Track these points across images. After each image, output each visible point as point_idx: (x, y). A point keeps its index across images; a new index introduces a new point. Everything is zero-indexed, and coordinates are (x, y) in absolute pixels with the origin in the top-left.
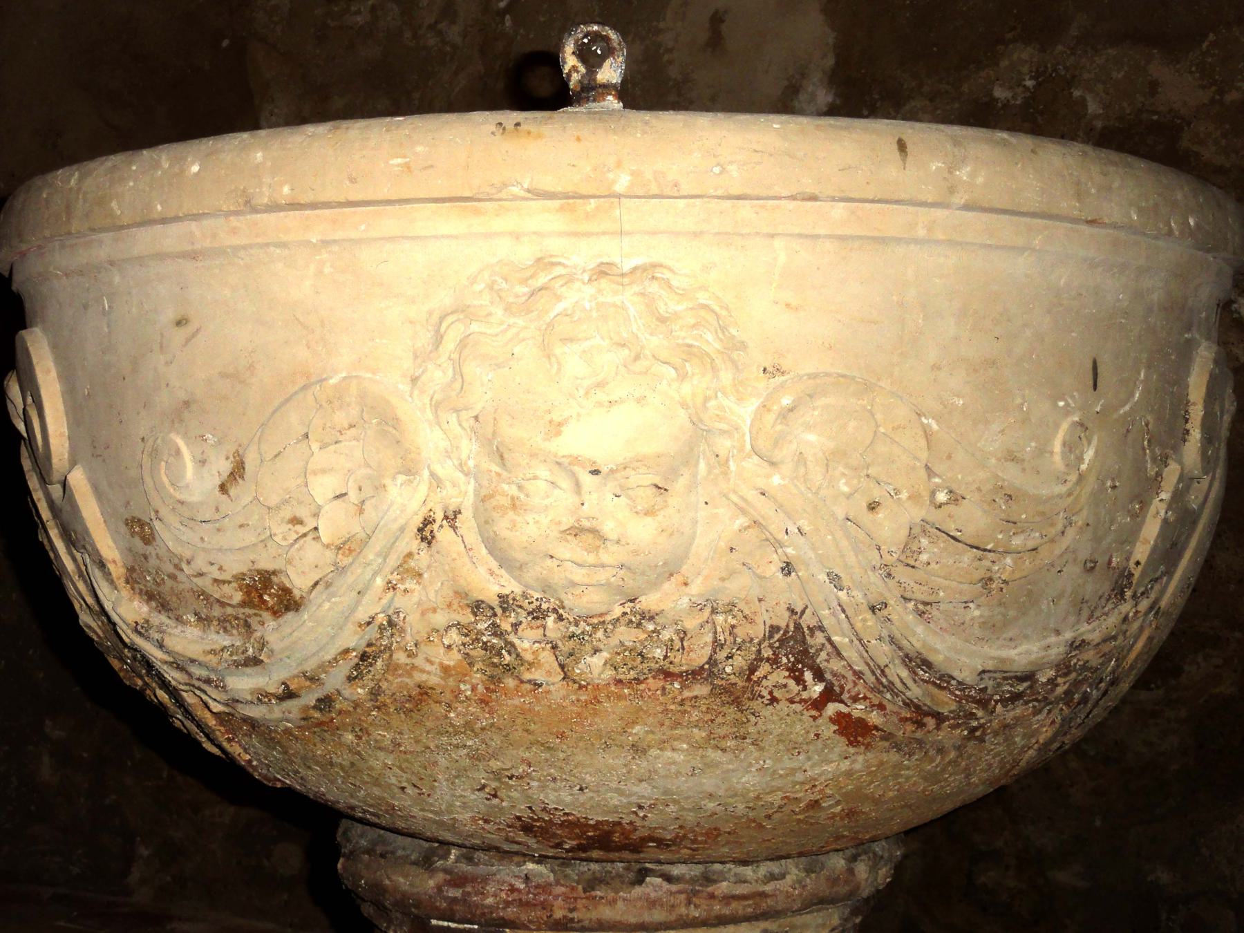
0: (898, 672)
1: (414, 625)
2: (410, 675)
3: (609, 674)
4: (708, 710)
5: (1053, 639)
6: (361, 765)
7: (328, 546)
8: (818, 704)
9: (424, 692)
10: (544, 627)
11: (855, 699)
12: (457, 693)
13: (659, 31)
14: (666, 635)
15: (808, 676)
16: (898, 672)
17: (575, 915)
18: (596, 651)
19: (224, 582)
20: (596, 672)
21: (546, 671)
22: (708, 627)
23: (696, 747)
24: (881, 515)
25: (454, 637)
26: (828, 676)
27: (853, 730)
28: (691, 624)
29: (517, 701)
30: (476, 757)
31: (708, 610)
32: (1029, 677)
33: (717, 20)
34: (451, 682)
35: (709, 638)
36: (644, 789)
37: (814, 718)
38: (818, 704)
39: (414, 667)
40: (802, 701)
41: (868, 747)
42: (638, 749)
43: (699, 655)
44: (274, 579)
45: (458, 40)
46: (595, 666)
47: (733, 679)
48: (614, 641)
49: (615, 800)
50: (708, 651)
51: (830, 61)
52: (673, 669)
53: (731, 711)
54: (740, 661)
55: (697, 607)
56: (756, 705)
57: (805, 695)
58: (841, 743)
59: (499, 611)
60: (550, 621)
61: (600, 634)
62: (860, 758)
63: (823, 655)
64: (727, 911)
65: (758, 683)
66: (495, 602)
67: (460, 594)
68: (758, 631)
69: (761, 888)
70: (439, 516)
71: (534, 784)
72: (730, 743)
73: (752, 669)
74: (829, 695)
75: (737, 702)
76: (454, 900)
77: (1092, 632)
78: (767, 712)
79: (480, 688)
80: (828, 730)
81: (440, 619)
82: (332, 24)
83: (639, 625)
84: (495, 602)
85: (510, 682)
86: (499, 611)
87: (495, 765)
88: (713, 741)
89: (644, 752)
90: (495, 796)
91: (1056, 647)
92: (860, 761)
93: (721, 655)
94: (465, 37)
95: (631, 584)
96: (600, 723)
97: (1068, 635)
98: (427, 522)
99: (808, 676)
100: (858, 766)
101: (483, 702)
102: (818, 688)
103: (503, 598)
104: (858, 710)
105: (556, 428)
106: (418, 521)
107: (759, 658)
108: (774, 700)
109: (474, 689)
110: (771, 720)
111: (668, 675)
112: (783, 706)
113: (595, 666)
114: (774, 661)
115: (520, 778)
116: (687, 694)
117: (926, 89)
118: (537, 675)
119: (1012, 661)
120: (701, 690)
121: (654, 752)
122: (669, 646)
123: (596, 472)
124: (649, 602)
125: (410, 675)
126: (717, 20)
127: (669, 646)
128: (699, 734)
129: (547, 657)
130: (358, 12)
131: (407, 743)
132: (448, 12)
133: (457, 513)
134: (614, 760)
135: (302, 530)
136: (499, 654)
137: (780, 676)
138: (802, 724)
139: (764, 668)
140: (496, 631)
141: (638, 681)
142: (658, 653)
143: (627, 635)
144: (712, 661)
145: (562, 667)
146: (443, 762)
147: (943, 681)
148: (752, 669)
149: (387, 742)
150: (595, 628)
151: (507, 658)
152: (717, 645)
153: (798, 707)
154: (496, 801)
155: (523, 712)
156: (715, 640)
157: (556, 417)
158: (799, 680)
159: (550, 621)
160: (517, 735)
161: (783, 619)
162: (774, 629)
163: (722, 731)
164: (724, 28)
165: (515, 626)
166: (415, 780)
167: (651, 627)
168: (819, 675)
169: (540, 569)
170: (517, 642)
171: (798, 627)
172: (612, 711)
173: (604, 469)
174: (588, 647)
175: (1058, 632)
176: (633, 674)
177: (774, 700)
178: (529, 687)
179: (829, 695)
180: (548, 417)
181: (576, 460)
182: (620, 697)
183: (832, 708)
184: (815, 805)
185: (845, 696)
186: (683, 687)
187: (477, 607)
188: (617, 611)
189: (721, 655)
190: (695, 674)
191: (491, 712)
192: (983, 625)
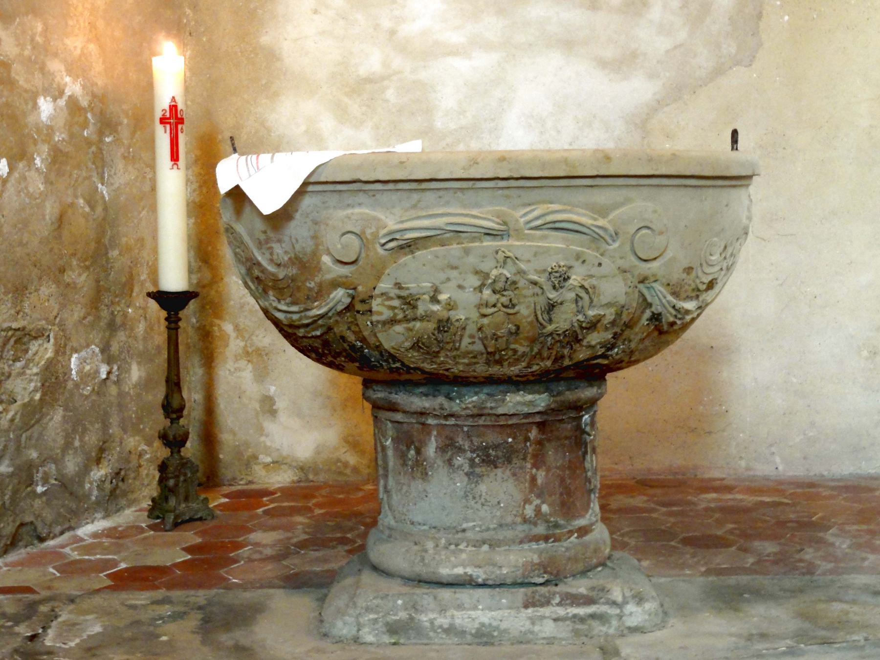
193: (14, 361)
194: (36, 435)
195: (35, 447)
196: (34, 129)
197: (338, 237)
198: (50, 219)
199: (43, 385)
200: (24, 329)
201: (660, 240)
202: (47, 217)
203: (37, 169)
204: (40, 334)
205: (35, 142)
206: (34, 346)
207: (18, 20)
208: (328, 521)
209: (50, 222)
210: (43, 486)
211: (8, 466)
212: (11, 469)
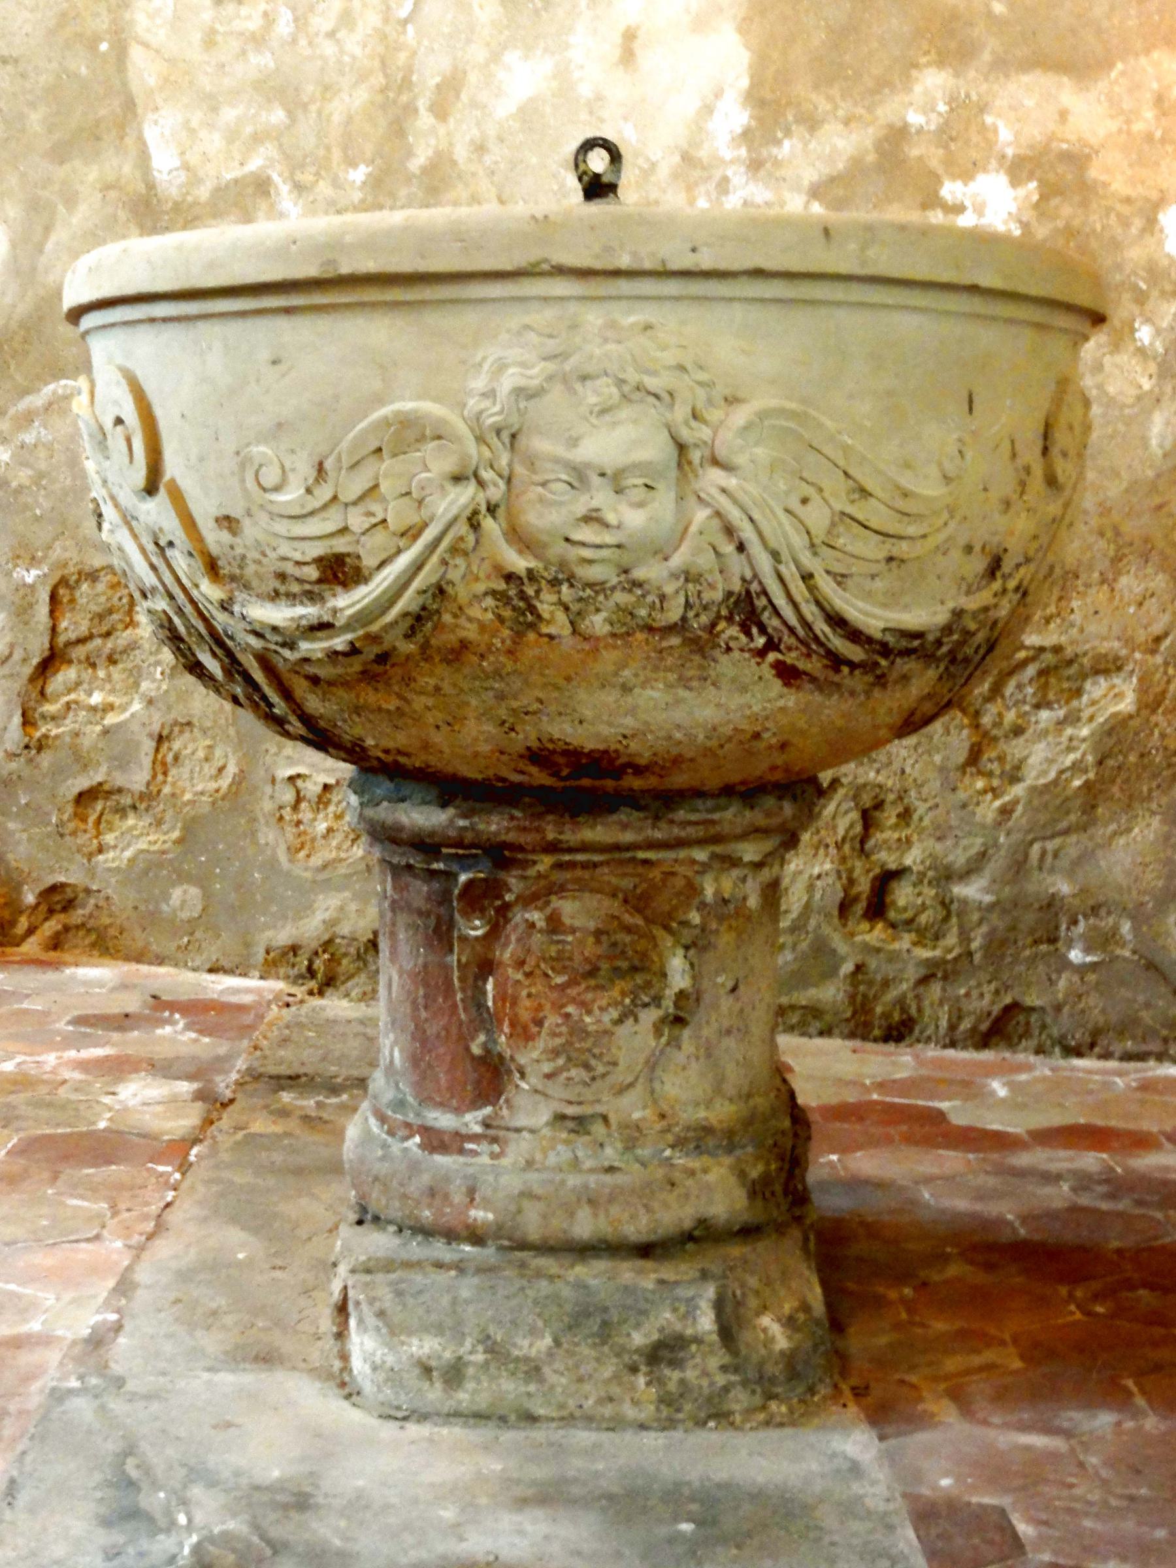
0: (821, 627)
1: (462, 593)
2: (453, 631)
3: (607, 628)
4: (680, 657)
5: (939, 608)
6: (407, 709)
7: (394, 534)
8: (761, 653)
9: (464, 645)
10: (559, 592)
11: (790, 649)
12: (490, 646)
13: (567, 46)
14: (650, 599)
15: (755, 630)
16: (821, 627)
17: (562, 837)
18: (598, 610)
19: (305, 564)
20: (597, 627)
21: (559, 624)
22: (682, 593)
23: (669, 686)
24: (809, 507)
25: (489, 602)
26: (770, 630)
27: (788, 674)
28: (669, 589)
29: (537, 651)
30: (501, 697)
31: (682, 579)
32: (919, 635)
33: (630, 36)
34: (486, 637)
35: (682, 600)
36: (629, 721)
37: (758, 664)
38: (761, 653)
39: (457, 626)
40: (750, 650)
41: (798, 688)
42: (626, 689)
43: (674, 614)
44: (348, 560)
45: (358, 51)
46: (598, 623)
47: (700, 633)
48: (611, 603)
49: (605, 730)
50: (681, 611)
51: (745, 83)
52: (655, 625)
53: (697, 658)
54: (704, 619)
55: (674, 576)
56: (717, 653)
57: (752, 645)
58: (778, 683)
59: (526, 580)
60: (565, 588)
61: (601, 598)
62: (793, 698)
63: (766, 614)
64: (683, 834)
65: (718, 635)
66: (523, 574)
67: (497, 568)
68: (718, 595)
69: (709, 816)
70: (483, 508)
71: (545, 718)
72: (695, 684)
73: (713, 625)
74: (771, 645)
75: (701, 651)
76: (465, 828)
77: (972, 603)
78: (724, 659)
79: (508, 642)
80: (767, 672)
81: (480, 587)
82: (221, 29)
83: (630, 591)
84: (523, 574)
85: (531, 636)
86: (526, 580)
87: (515, 704)
88: (684, 681)
89: (631, 690)
90: (512, 729)
91: (941, 617)
92: (791, 699)
93: (691, 614)
94: (365, 46)
95: (626, 558)
96: (598, 668)
97: (951, 605)
98: (475, 513)
99: (755, 630)
100: (791, 704)
101: (510, 652)
102: (761, 641)
103: (530, 571)
104: (791, 658)
105: (574, 442)
106: (468, 512)
107: (719, 617)
108: (729, 649)
109: (503, 642)
110: (725, 666)
111: (650, 629)
112: (736, 654)
113: (598, 623)
114: (730, 619)
115: (535, 713)
116: (665, 644)
117: (840, 113)
118: (551, 630)
119: (1000, 1222)
120: (675, 641)
121: (637, 691)
122: (652, 606)
123: (603, 475)
124: (639, 574)
125: (453, 631)
126: (630, 36)
127: (652, 606)
128: (672, 677)
129: (561, 616)
130: (249, 17)
131: (446, 687)
132: (347, 19)
133: (497, 506)
134: (610, 697)
135: (374, 520)
136: (524, 614)
137: (734, 631)
138: (750, 669)
139: (722, 625)
140: (522, 596)
141: (628, 634)
142: (643, 612)
143: (621, 597)
144: (684, 619)
145: (572, 623)
146: (474, 702)
147: (855, 635)
148: (713, 625)
149: (430, 688)
150: (597, 592)
151: (530, 618)
152: (688, 605)
153: (747, 655)
154: (513, 734)
155: (540, 659)
156: (687, 601)
157: (573, 433)
158: (748, 634)
159: (565, 588)
160: (534, 678)
161: (737, 587)
162: (730, 594)
163: (690, 673)
164: (637, 45)
165: (538, 592)
166: (450, 719)
167: (639, 592)
168: (763, 630)
169: (558, 549)
170: (538, 605)
171: (748, 592)
172: (610, 657)
173: (609, 472)
174: (592, 608)
175: (942, 603)
176: (624, 630)
177: (729, 649)
178: (546, 639)
179: (771, 645)
180: (567, 435)
181: (588, 465)
182: (615, 647)
183: (772, 656)
184: (757, 736)
185: (782, 647)
186: (662, 639)
187: (509, 577)
188: (614, 580)
189: (691, 614)
190: (671, 629)
191: (515, 661)
192: (885, 594)
193: (1037, 707)
194: (1073, 852)
195: (1070, 874)
196: (1143, 273)
197: (547, 399)
198: (1161, 446)
199: (1100, 763)
200: (1057, 649)
201: (890, 970)
202: (1154, 442)
203: (1141, 352)
204: (1107, 666)
205: (1141, 298)
206: (1096, 688)
207: (1120, 66)
208: (1071, 1475)
209: (1160, 452)
210: (1087, 950)
211: (987, 891)
212: (988, 899)
